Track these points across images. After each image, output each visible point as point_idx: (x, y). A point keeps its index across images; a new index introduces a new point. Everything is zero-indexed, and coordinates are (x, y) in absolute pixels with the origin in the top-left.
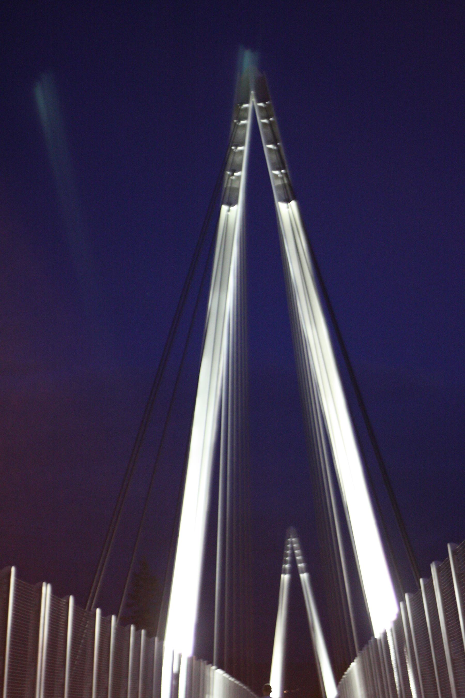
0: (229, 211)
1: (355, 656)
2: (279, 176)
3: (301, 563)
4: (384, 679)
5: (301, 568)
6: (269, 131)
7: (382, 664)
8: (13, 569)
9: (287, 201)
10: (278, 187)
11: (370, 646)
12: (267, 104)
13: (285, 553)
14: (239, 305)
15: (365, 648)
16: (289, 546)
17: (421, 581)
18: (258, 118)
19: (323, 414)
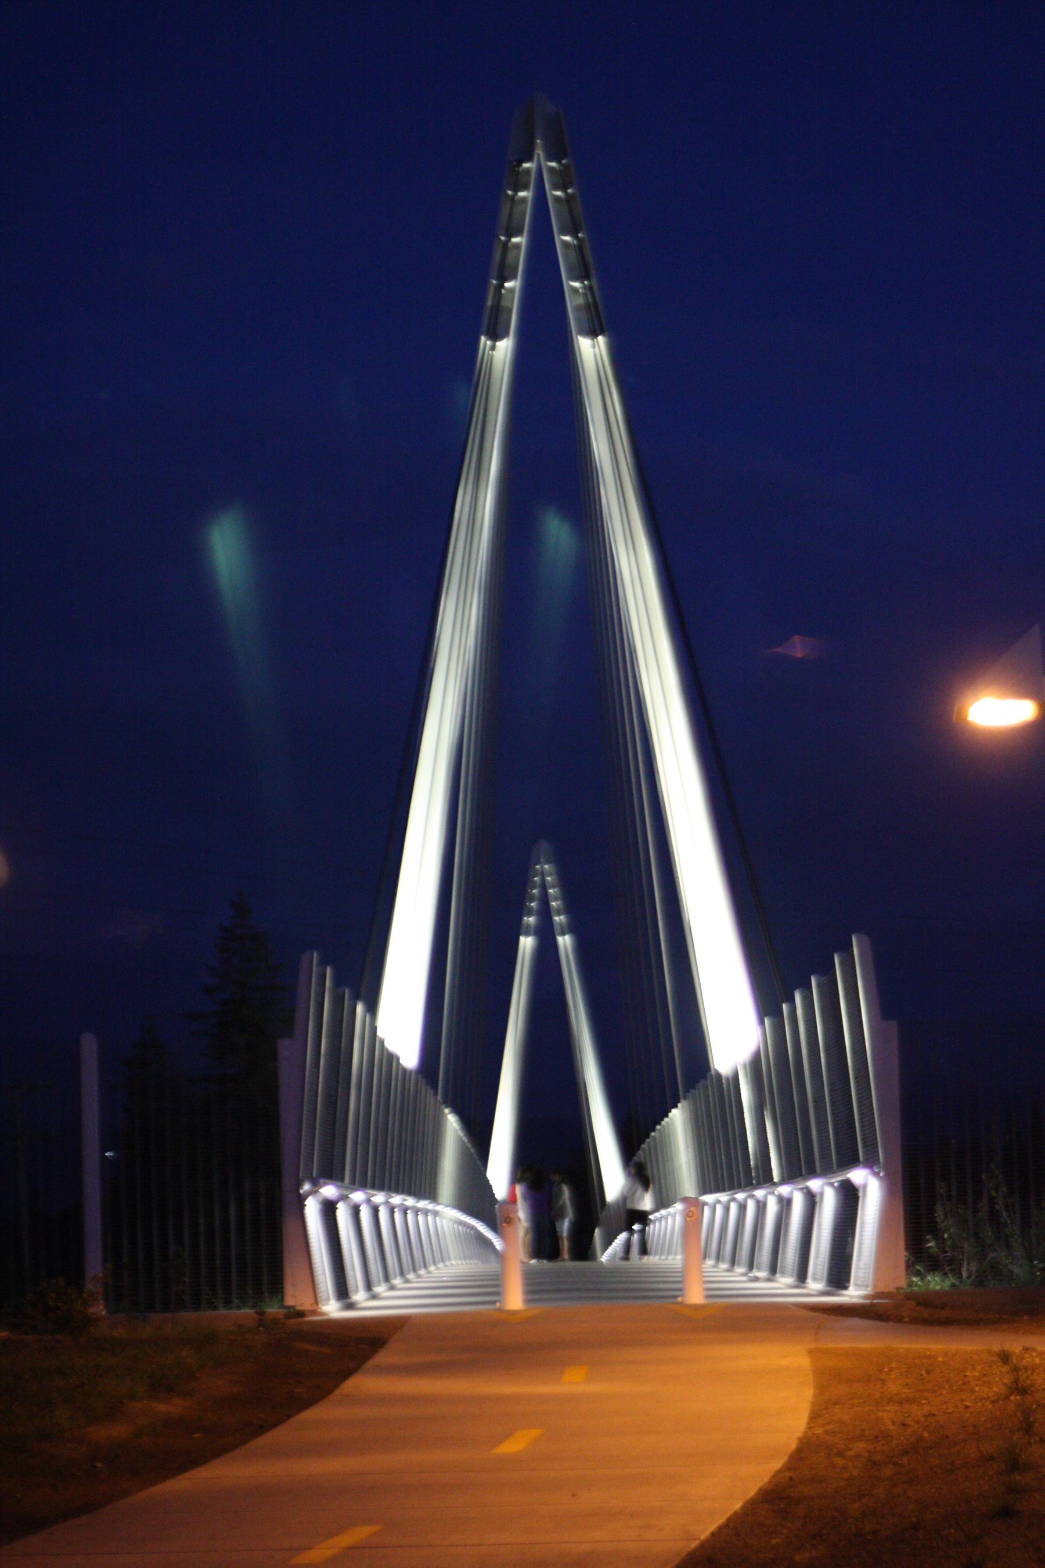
0: (493, 348)
2: (580, 291)
3: (559, 914)
4: (730, 1129)
5: (561, 924)
6: (573, 255)
9: (593, 334)
13: (528, 893)
15: (700, 1085)
17: (784, 1006)
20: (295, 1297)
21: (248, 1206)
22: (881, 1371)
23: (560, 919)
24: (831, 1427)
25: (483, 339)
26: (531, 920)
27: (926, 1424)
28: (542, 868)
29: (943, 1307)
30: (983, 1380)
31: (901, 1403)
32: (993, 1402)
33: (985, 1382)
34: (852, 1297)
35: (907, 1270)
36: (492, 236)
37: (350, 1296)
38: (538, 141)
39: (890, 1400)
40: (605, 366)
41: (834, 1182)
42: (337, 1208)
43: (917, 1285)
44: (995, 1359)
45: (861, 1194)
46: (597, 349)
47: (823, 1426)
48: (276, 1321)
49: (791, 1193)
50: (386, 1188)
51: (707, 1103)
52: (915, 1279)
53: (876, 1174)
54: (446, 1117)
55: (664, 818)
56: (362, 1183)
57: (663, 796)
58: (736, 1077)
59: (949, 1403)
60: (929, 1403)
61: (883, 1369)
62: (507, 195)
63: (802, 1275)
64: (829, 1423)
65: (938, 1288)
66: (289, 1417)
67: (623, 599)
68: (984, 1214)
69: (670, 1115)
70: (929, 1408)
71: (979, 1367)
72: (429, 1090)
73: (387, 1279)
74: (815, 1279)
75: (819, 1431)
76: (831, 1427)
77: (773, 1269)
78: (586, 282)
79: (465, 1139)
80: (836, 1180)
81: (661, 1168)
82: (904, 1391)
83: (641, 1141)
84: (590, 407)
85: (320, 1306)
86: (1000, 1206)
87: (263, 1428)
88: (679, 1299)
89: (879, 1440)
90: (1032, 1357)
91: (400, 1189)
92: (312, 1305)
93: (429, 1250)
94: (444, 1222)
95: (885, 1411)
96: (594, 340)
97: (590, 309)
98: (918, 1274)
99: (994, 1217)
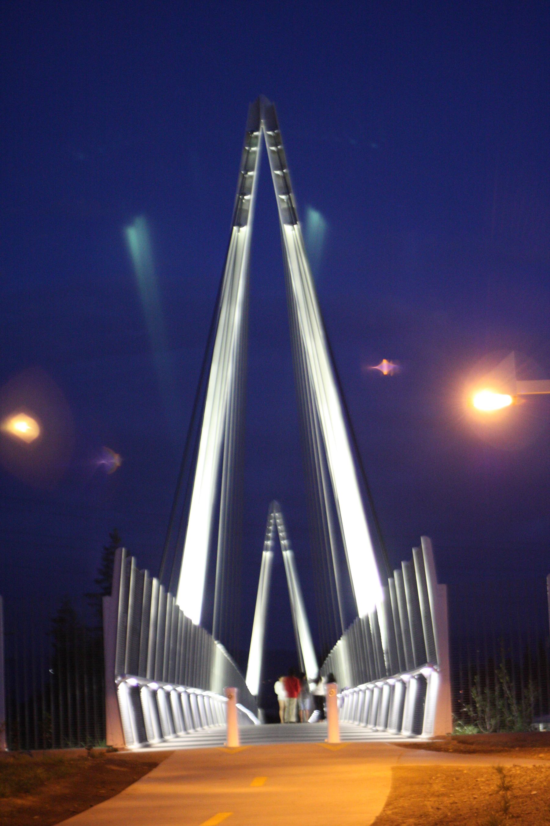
0: (239, 231)
5: (285, 546)
6: (281, 181)
12: (275, 133)
13: (267, 528)
16: (272, 521)
18: (267, 145)
19: (320, 420)
20: (112, 740)
21: (86, 690)
22: (431, 778)
23: (284, 543)
24: (396, 810)
27: (451, 808)
29: (472, 744)
30: (486, 783)
31: (438, 796)
32: (491, 795)
33: (487, 784)
34: (422, 739)
35: (453, 724)
36: (238, 171)
37: (148, 740)
38: (262, 121)
39: (433, 795)
41: (415, 676)
42: (118, 689)
43: (459, 732)
44: (495, 771)
45: (428, 682)
47: (392, 809)
48: (102, 754)
49: (395, 683)
50: (163, 680)
51: (354, 633)
52: (457, 729)
53: (436, 670)
54: (216, 646)
56: (159, 678)
57: (331, 472)
59: (465, 796)
60: (454, 796)
61: (432, 777)
62: (246, 149)
63: (400, 728)
64: (396, 808)
65: (470, 733)
66: (92, 806)
68: (497, 693)
69: (337, 644)
70: (454, 799)
71: (485, 776)
72: (204, 631)
73: (174, 731)
74: (406, 730)
75: (389, 812)
76: (396, 810)
77: (386, 726)
79: (229, 659)
80: (416, 673)
82: (441, 789)
83: (325, 659)
84: (291, 264)
85: (126, 745)
86: (505, 688)
87: (75, 813)
88: (326, 740)
89: (422, 818)
90: (516, 770)
91: (176, 680)
92: (122, 745)
93: (204, 717)
94: (216, 703)
95: (429, 801)
97: (290, 210)
98: (459, 725)
99: (502, 694)
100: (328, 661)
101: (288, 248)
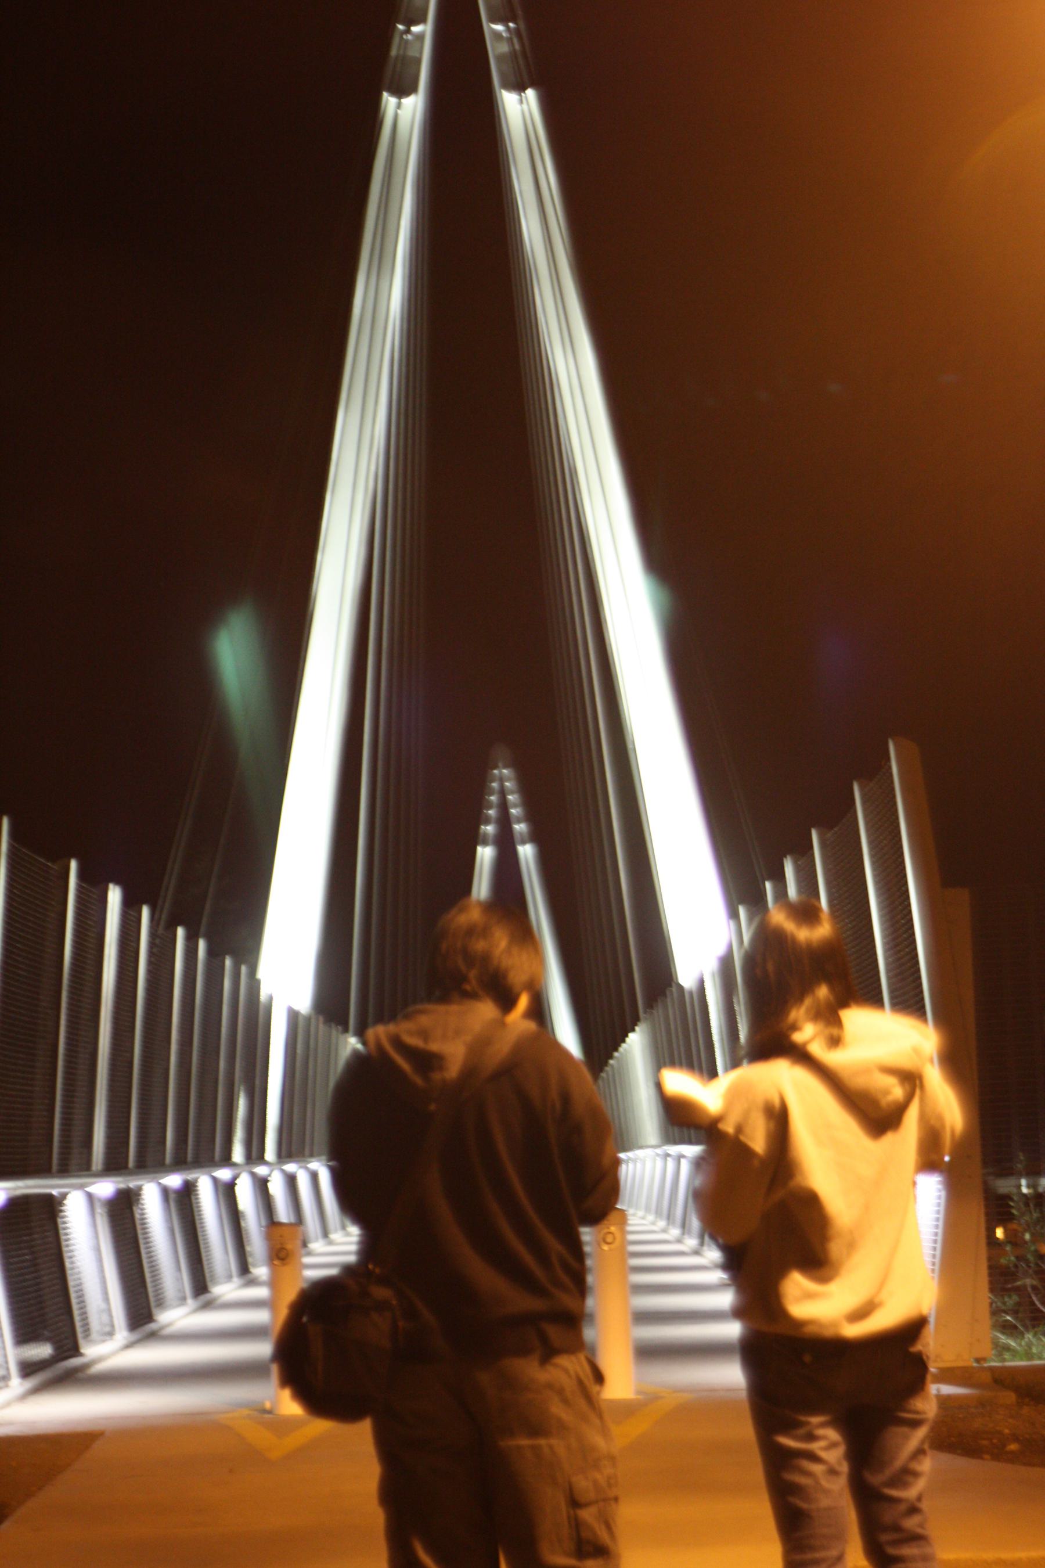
0: (399, 106)
1: (635, 1021)
2: (504, 35)
5: (521, 834)
7: (692, 1034)
8: (73, 865)
10: (500, 59)
11: (669, 1000)
14: (413, 299)
25: (385, 94)
26: (489, 829)
28: (501, 773)
40: (536, 124)
46: (525, 106)
51: (667, 1024)
55: (610, 658)
58: (701, 983)
67: (565, 432)
69: (627, 1040)
78: (511, 25)
81: (619, 1093)
83: (605, 1063)
96: (521, 96)
100: (608, 1075)
101: (513, 151)
